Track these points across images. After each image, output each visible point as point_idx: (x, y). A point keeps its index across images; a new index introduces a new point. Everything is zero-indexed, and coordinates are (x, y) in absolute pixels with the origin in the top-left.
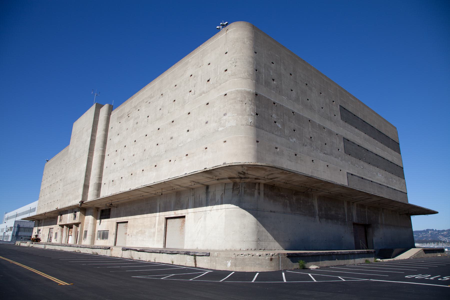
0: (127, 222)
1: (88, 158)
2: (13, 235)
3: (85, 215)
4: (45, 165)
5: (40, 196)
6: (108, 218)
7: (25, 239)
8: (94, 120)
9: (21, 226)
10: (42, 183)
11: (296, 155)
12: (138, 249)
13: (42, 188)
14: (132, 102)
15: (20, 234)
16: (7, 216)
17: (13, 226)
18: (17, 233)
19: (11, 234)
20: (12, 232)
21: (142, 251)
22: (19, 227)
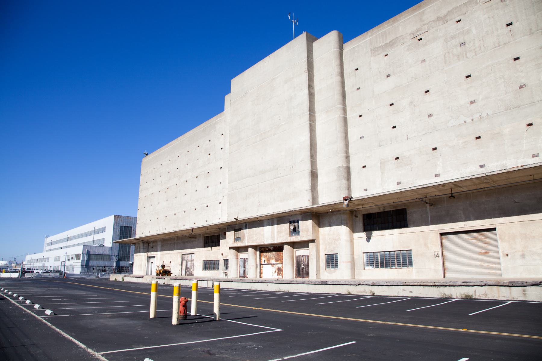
0: (494, 229)
1: (310, 125)
2: (82, 265)
3: (320, 227)
4: (141, 161)
5: (139, 206)
6: (405, 226)
7: (98, 271)
8: (308, 60)
9: (92, 253)
10: (141, 187)
11: (221, 183)
12: (491, 283)
13: (141, 195)
14: (423, 13)
15: (91, 263)
16: (49, 240)
17: (81, 252)
18: (88, 261)
19: (80, 264)
20: (80, 261)
21: (373, 285)
22: (89, 254)
